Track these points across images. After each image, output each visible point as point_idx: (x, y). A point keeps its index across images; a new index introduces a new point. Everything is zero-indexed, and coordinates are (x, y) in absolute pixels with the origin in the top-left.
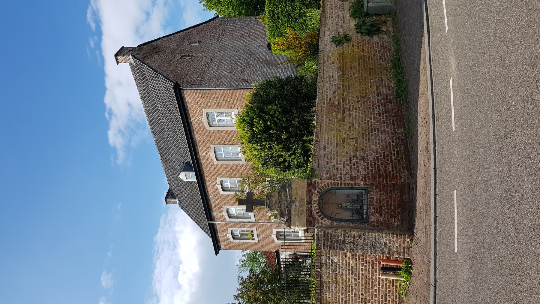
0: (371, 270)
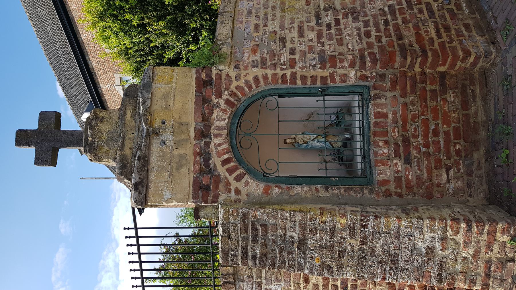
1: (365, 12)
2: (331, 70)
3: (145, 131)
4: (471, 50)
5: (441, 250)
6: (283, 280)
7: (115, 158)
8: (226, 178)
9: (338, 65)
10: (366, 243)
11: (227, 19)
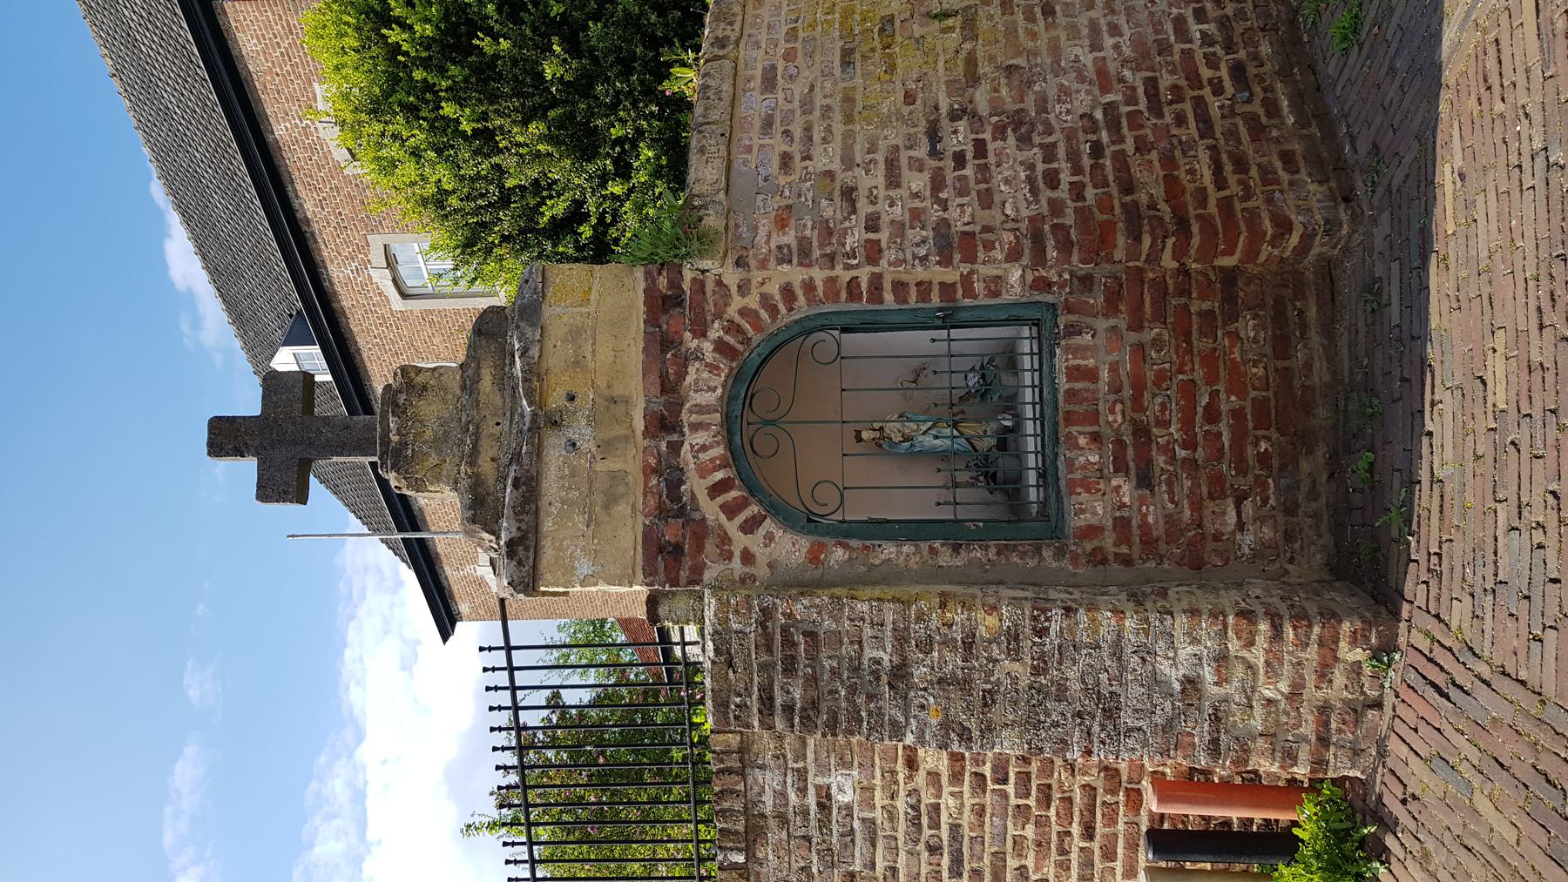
0: (1077, 842)
1: (1047, 123)
2: (965, 268)
3: (527, 419)
4: (1293, 217)
5: (1216, 684)
6: (856, 763)
7: (456, 482)
8: (720, 526)
9: (981, 255)
10: (1045, 671)
11: (713, 142)
